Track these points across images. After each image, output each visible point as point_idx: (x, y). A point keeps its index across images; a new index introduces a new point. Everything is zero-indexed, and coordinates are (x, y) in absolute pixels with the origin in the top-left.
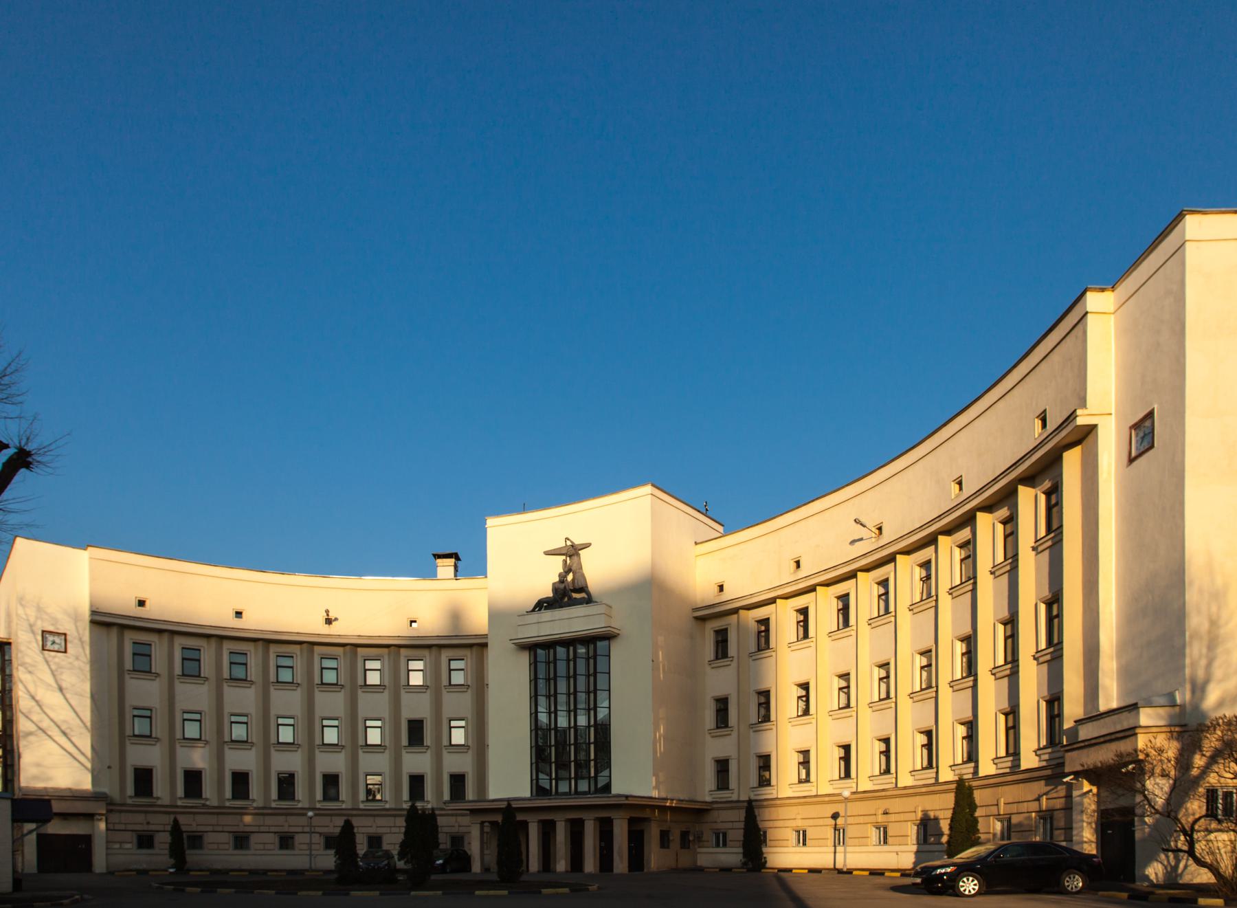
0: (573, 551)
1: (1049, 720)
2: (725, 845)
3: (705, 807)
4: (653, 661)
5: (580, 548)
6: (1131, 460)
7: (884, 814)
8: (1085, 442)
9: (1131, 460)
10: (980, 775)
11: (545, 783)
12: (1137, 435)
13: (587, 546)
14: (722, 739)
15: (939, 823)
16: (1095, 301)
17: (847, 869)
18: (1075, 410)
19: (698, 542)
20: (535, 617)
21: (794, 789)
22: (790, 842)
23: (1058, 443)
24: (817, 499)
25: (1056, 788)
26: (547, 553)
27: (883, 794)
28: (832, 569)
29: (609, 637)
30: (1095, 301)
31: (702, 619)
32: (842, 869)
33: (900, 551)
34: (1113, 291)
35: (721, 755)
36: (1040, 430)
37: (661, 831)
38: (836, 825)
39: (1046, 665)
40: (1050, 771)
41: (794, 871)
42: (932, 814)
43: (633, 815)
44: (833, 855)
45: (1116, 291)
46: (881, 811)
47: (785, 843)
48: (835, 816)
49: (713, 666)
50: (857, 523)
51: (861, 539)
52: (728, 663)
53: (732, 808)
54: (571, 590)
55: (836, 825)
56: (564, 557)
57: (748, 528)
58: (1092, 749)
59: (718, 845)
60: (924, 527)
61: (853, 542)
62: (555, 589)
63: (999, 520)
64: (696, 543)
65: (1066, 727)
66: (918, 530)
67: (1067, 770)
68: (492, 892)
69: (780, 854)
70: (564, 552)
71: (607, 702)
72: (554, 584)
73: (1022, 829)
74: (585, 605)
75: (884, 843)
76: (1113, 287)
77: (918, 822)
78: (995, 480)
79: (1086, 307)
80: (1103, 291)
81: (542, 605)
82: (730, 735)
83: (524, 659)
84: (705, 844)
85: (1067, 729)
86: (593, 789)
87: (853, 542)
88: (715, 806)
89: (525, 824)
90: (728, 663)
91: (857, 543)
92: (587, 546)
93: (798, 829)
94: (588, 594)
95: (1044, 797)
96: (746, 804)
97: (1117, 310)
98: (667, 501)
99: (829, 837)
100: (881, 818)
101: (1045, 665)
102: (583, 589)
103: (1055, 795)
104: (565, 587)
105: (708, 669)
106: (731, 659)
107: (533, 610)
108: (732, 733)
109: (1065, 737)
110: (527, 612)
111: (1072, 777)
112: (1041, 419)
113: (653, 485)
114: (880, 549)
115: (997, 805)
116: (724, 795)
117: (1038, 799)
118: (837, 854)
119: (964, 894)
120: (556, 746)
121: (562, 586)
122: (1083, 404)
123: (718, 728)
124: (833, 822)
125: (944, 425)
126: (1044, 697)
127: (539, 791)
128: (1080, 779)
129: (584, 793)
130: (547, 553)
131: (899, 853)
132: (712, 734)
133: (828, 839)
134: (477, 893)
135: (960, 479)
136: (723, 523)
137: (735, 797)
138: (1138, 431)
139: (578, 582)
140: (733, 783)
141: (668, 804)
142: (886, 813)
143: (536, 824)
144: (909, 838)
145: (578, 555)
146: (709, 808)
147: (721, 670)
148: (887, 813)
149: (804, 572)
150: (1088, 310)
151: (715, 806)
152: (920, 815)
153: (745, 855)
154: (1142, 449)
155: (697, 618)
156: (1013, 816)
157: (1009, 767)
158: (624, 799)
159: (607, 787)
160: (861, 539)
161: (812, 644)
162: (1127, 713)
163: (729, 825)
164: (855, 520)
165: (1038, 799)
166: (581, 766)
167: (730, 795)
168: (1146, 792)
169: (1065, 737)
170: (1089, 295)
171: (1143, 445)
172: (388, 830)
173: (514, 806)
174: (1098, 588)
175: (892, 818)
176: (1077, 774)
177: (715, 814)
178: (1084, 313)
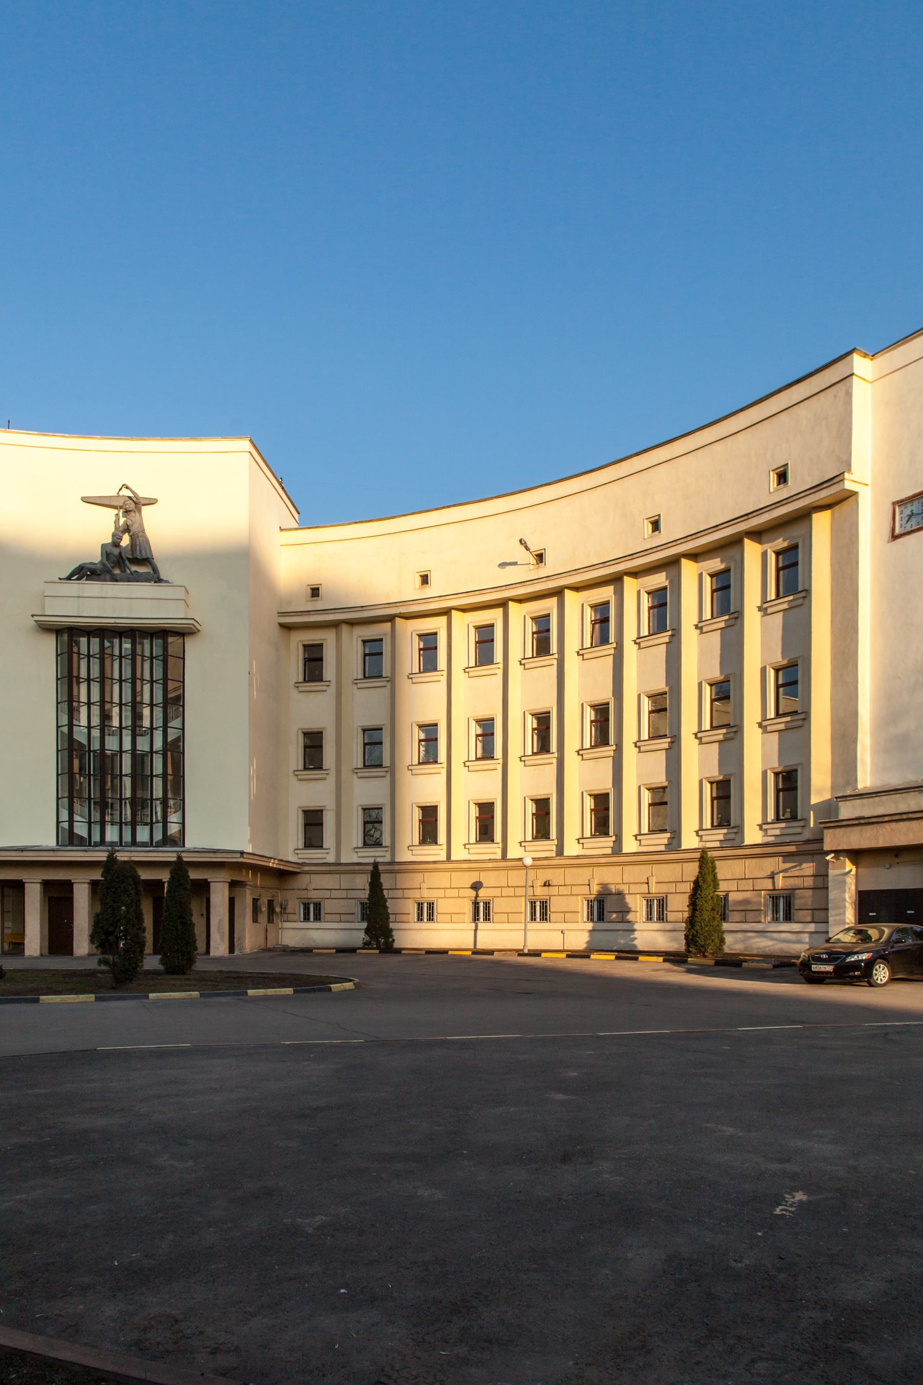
0: (132, 506)
1: (776, 792)
2: (318, 918)
3: (291, 869)
4: (249, 674)
5: (143, 503)
6: (894, 537)
7: (545, 885)
8: (836, 508)
9: (894, 537)
10: (683, 848)
11: (81, 829)
12: (901, 513)
13: (152, 502)
14: (313, 784)
15: (624, 898)
16: (860, 364)
17: (529, 950)
18: (843, 473)
19: (282, 528)
20: (74, 588)
21: (360, 854)
22: (411, 916)
23: (810, 503)
24: (455, 505)
25: (800, 865)
26: (86, 500)
27: (546, 862)
28: (477, 593)
29: (184, 633)
30: (860, 364)
31: (287, 628)
32: (522, 950)
33: (571, 586)
34: (872, 359)
35: (313, 804)
36: (775, 486)
37: (254, 899)
38: (477, 896)
39: (776, 736)
40: (794, 847)
41: (450, 953)
42: (613, 889)
43: (234, 878)
44: (472, 933)
45: (874, 361)
46: (540, 882)
47: (404, 918)
48: (476, 886)
49: (301, 689)
50: (521, 544)
51: (515, 564)
52: (325, 688)
53: (330, 872)
54: (128, 558)
55: (477, 896)
56: (116, 511)
57: (356, 523)
58: (868, 827)
59: (306, 918)
60: (608, 564)
61: (503, 565)
62: (106, 551)
63: (708, 572)
64: (281, 530)
65: (815, 800)
66: (600, 566)
67: (826, 847)
68: (271, 992)
69: (409, 932)
70: (116, 504)
71: (179, 720)
72: (104, 546)
73: (749, 907)
74: (153, 583)
75: (418, 920)
76: (873, 356)
77: (594, 896)
78: (716, 528)
79: (852, 369)
80: (864, 357)
81: (84, 573)
82: (325, 779)
83: (49, 645)
84: (291, 917)
85: (814, 804)
86: (158, 836)
87: (503, 565)
88: (306, 868)
89: (203, 888)
90: (325, 688)
91: (509, 567)
92: (152, 502)
93: (421, 901)
94: (155, 570)
95: (781, 874)
96: (371, 868)
97: (875, 380)
98: (264, 470)
99: (580, 911)
100: (540, 892)
101: (775, 736)
102: (147, 561)
103: (797, 874)
104: (120, 553)
105: (294, 692)
106: (327, 683)
107: (69, 578)
108: (328, 777)
109: (812, 812)
110: (60, 579)
111: (833, 855)
112: (777, 474)
113: (251, 441)
114: (545, 579)
115: (648, 883)
116: (313, 855)
117: (772, 877)
118: (478, 932)
119: (876, 982)
120: (134, 775)
121: (116, 551)
122: (849, 470)
123: (305, 769)
124: (473, 893)
125: (637, 454)
126: (774, 768)
127: (70, 838)
128: (842, 858)
129: (144, 844)
130: (86, 500)
131: (566, 932)
132: (299, 777)
133: (579, 912)
134: (251, 992)
135: (657, 518)
136: (299, 510)
137: (331, 858)
138: (902, 508)
139: (140, 551)
140: (329, 839)
141: (271, 865)
142: (547, 884)
143: (86, 886)
144: (638, 913)
145: (140, 511)
146: (298, 870)
147: (312, 695)
148: (549, 885)
149: (431, 591)
150: (855, 371)
151: (306, 868)
152: (595, 889)
153: (367, 931)
154: (908, 529)
155: (283, 626)
156: (730, 894)
157: (720, 841)
158: (239, 855)
159: (178, 841)
160: (515, 564)
161: (441, 678)
162: (917, 792)
163: (327, 894)
164: (521, 541)
165: (772, 877)
166: (139, 804)
167: (325, 856)
168: (775, 872)
169: (812, 812)
170: (856, 357)
171: (909, 523)
172: (497, 892)
173: (185, 859)
174: (857, 661)
175: (554, 891)
176: (838, 853)
177: (303, 881)
178: (851, 373)
